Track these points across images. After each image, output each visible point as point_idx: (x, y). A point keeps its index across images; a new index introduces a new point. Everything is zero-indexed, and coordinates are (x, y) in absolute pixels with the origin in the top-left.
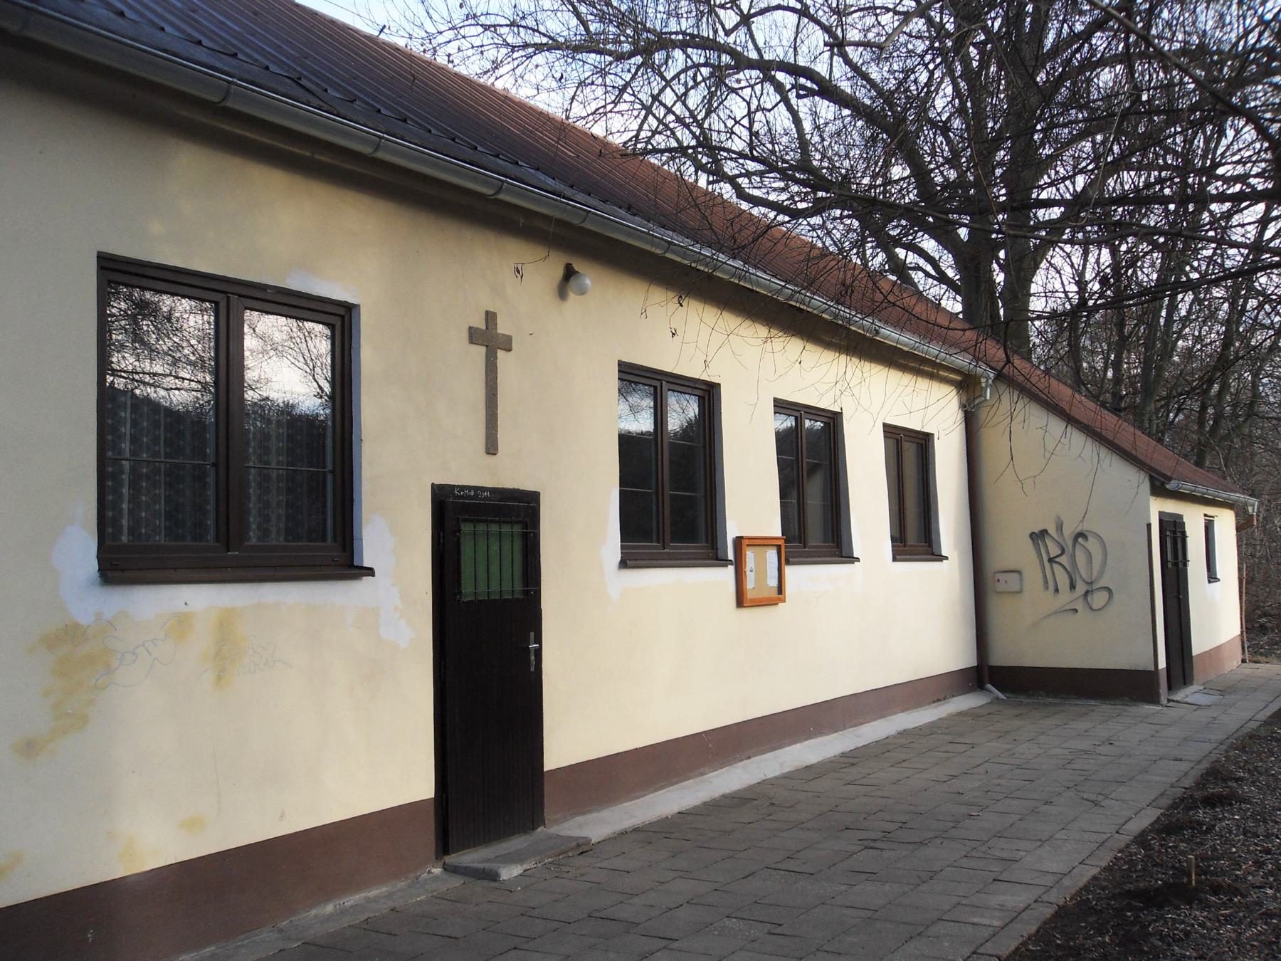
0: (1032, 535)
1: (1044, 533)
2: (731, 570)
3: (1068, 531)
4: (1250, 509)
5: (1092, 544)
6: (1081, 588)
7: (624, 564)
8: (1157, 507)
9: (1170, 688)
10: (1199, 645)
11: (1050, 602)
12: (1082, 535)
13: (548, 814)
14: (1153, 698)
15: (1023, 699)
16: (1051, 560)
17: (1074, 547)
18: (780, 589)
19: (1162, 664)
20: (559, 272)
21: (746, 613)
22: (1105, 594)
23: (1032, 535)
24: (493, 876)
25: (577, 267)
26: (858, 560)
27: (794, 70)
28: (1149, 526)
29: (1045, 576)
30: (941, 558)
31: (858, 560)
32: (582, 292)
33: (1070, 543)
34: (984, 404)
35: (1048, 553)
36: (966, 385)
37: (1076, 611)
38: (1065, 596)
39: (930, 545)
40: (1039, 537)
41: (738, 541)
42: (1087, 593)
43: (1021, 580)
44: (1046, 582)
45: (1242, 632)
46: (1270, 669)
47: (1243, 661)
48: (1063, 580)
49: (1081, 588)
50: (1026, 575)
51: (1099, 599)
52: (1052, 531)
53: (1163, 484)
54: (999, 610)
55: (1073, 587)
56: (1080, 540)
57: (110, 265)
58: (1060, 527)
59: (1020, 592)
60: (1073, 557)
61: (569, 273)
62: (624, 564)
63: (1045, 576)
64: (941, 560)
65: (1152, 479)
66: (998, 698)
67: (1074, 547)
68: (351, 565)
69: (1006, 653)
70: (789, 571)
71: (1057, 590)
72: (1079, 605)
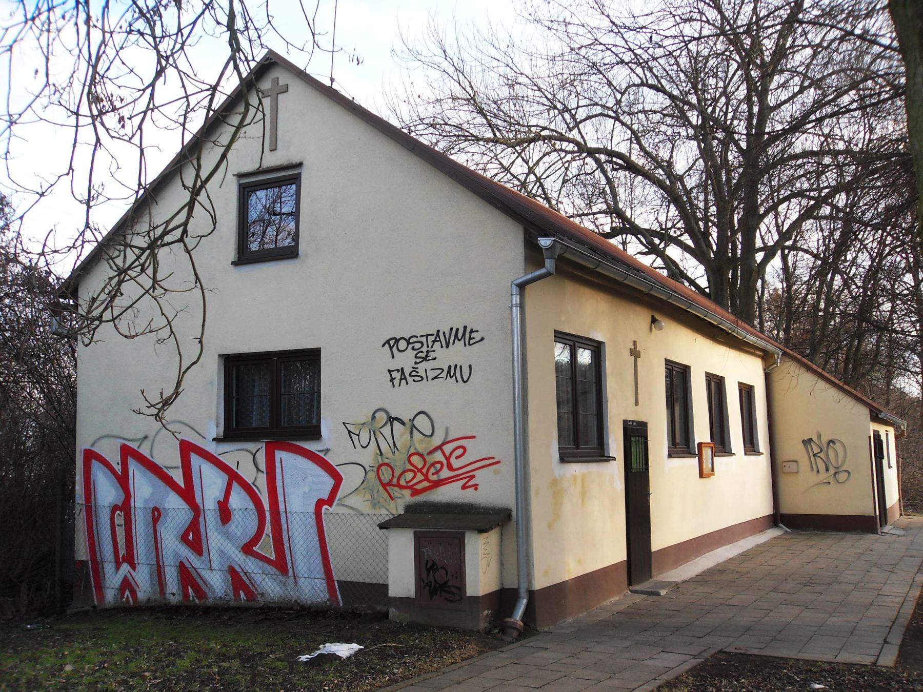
0: (803, 441)
1: (810, 440)
2: (695, 461)
3: (824, 440)
4: (902, 427)
5: (838, 446)
6: (832, 471)
7: (670, 456)
8: (874, 426)
9: (881, 526)
10: (888, 506)
11: (814, 478)
12: (831, 441)
13: (654, 573)
14: (874, 531)
15: (800, 532)
16: (814, 455)
17: (828, 448)
18: (713, 470)
19: (878, 513)
20: (649, 320)
21: (702, 480)
22: (846, 475)
23: (803, 441)
24: (658, 594)
25: (657, 317)
26: (734, 454)
27: (611, 153)
28: (870, 437)
29: (811, 464)
30: (760, 454)
31: (734, 454)
32: (661, 329)
33: (825, 446)
34: (776, 369)
35: (813, 451)
36: (766, 356)
37: (829, 483)
38: (823, 475)
39: (724, 447)
40: (807, 442)
41: (700, 445)
42: (836, 473)
43: (798, 465)
44: (812, 467)
45: (899, 500)
46: (918, 519)
47: (901, 515)
48: (822, 467)
49: (832, 471)
50: (800, 464)
51: (842, 477)
52: (815, 439)
53: (877, 414)
54: (786, 483)
55: (827, 470)
56: (831, 444)
57: (560, 336)
58: (819, 437)
59: (797, 473)
60: (827, 455)
61: (654, 321)
62: (670, 456)
63: (811, 464)
64: (608, 461)
65: (871, 411)
66: (786, 531)
67: (828, 448)
68: (604, 456)
69: (790, 506)
70: (715, 459)
71: (818, 472)
72: (831, 480)
